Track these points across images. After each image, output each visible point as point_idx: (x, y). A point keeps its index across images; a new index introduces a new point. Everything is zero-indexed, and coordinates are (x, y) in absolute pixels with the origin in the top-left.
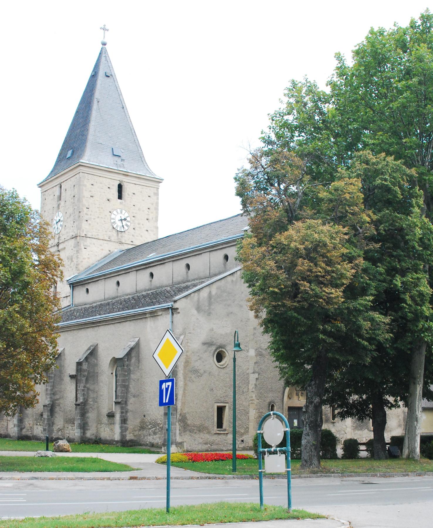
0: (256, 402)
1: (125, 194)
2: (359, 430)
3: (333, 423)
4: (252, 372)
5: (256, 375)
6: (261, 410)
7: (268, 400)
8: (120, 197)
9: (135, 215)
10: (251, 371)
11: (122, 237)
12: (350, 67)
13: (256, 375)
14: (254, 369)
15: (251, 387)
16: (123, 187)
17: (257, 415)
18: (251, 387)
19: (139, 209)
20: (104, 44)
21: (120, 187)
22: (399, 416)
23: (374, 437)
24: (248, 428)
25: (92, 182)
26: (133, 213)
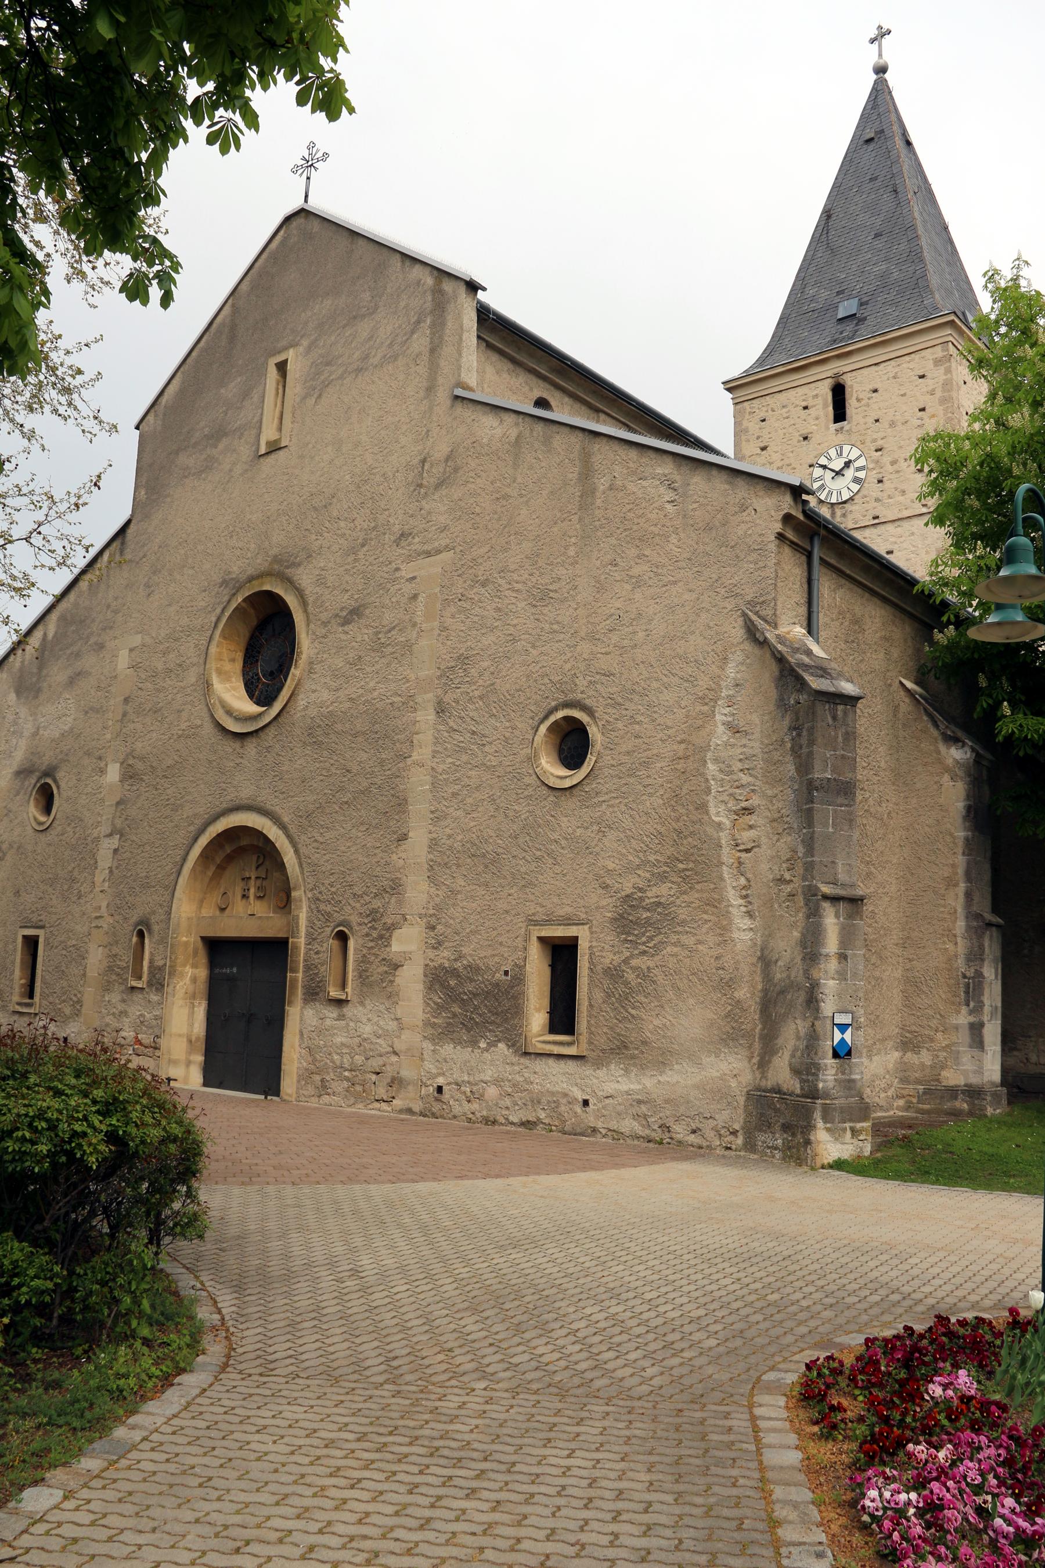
0: (106, 923)
1: (852, 405)
2: (458, 1042)
3: (340, 1003)
4: (108, 831)
5: (115, 842)
6: (115, 950)
7: (134, 919)
8: (840, 414)
9: (880, 443)
10: (105, 829)
11: (844, 515)
12: (47, 279)
13: (115, 842)
14: (113, 824)
15: (101, 876)
16: (848, 390)
17: (105, 964)
18: (101, 876)
19: (893, 424)
20: (881, 70)
21: (839, 393)
22: (728, 985)
23: (1028, 1189)
24: (79, 1001)
25: (762, 415)
26: (875, 441)
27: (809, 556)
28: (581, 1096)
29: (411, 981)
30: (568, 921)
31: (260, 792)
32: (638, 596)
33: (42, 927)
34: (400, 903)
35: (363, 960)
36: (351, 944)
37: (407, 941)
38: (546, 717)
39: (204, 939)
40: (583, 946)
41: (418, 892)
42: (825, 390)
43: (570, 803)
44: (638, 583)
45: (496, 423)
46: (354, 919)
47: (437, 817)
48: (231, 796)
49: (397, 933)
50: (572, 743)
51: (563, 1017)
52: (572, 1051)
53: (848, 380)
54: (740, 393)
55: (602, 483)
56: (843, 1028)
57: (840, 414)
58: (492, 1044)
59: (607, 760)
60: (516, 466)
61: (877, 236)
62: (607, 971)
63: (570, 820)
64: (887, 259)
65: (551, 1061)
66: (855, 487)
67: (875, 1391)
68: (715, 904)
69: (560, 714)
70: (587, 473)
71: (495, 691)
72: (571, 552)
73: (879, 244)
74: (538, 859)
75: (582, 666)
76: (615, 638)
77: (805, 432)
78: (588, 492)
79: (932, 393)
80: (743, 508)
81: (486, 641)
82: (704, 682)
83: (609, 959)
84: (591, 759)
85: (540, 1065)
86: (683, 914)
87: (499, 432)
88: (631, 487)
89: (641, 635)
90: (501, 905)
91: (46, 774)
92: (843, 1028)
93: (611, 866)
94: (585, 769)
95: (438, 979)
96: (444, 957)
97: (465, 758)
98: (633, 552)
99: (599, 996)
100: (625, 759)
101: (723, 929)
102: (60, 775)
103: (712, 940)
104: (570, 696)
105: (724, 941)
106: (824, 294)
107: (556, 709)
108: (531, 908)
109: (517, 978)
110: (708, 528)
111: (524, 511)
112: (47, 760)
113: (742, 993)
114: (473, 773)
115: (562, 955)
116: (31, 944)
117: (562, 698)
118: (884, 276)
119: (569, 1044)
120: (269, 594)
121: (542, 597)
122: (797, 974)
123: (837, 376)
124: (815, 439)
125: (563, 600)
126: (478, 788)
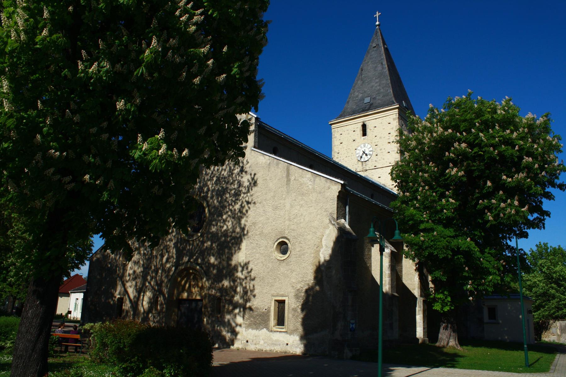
1: (368, 131)
2: (253, 329)
8: (364, 134)
9: (376, 144)
21: (364, 127)
30: (282, 296)
32: (301, 209)
38: (277, 241)
40: (286, 302)
43: (284, 264)
44: (302, 206)
45: (263, 158)
50: (283, 247)
52: (284, 330)
55: (292, 178)
56: (353, 324)
57: (364, 134)
58: (263, 328)
59: (293, 253)
60: (269, 171)
62: (293, 309)
63: (283, 268)
64: (379, 85)
65: (278, 333)
67: (272, 194)
69: (281, 240)
70: (288, 175)
71: (263, 233)
72: (284, 196)
74: (275, 279)
75: (287, 227)
76: (295, 220)
77: (354, 139)
78: (289, 180)
79: (392, 129)
80: (329, 188)
81: (260, 219)
82: (319, 234)
84: (289, 253)
87: (264, 161)
88: (300, 180)
89: (302, 220)
90: (265, 291)
92: (353, 324)
93: (294, 281)
97: (255, 251)
98: (300, 198)
99: (291, 316)
100: (298, 253)
104: (284, 235)
108: (273, 292)
109: (269, 311)
110: (320, 193)
111: (271, 184)
114: (257, 255)
117: (281, 236)
119: (283, 328)
121: (276, 208)
123: (363, 122)
124: (357, 141)
125: (282, 209)
126: (258, 259)
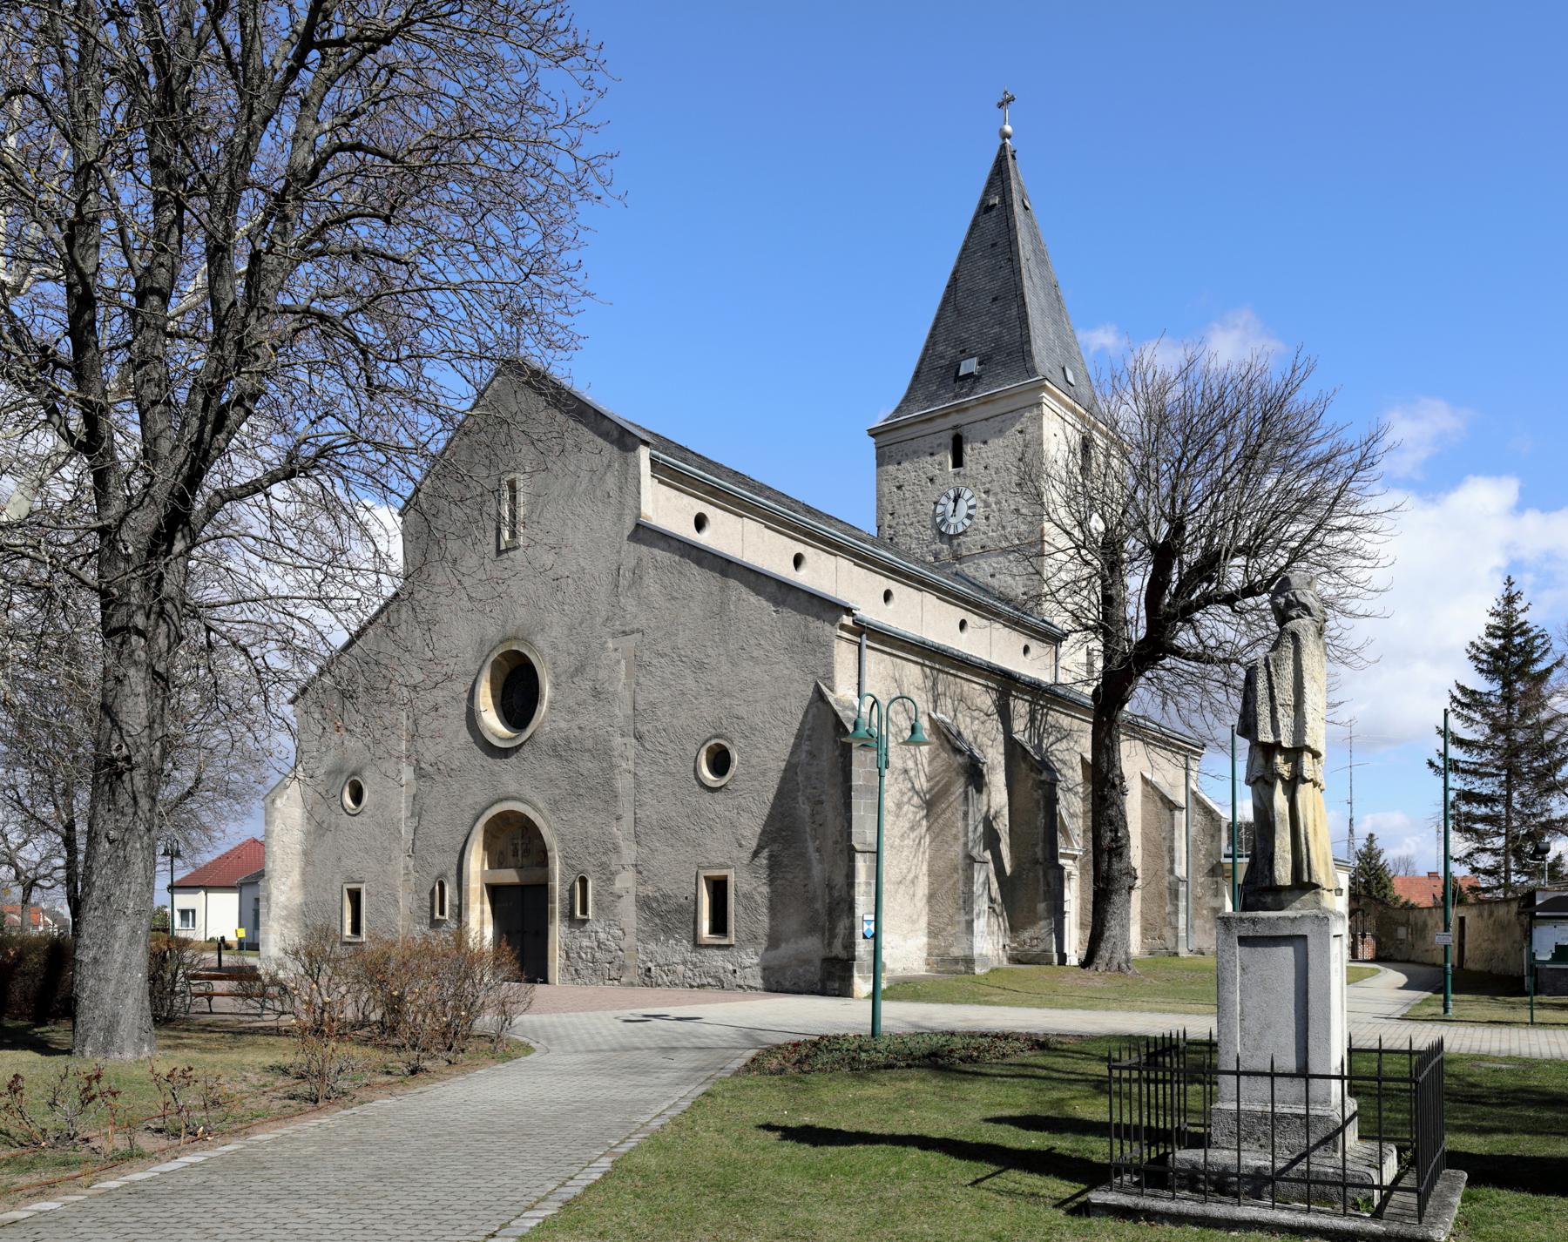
2: (657, 940)
22: (810, 901)
27: (860, 646)
28: (731, 968)
29: (628, 912)
30: (722, 866)
31: (526, 789)
33: (728, 867)
34: (619, 858)
35: (598, 894)
36: (590, 884)
37: (625, 881)
39: (488, 886)
41: (629, 852)
42: (947, 438)
46: (590, 869)
47: (639, 804)
48: (501, 792)
49: (618, 878)
51: (719, 926)
53: (965, 432)
54: (881, 438)
61: (995, 299)
63: (717, 806)
66: (967, 522)
68: (802, 855)
69: (713, 742)
73: (995, 308)
83: (746, 888)
85: (708, 952)
86: (786, 862)
90: (681, 857)
91: (354, 774)
94: (728, 776)
95: (644, 903)
96: (649, 890)
101: (807, 869)
102: (366, 774)
103: (801, 875)
105: (808, 877)
106: (951, 352)
107: (709, 739)
108: (700, 859)
112: (352, 764)
113: (818, 905)
115: (718, 889)
116: (355, 897)
118: (997, 339)
120: (517, 652)
122: (844, 894)
123: (955, 427)
